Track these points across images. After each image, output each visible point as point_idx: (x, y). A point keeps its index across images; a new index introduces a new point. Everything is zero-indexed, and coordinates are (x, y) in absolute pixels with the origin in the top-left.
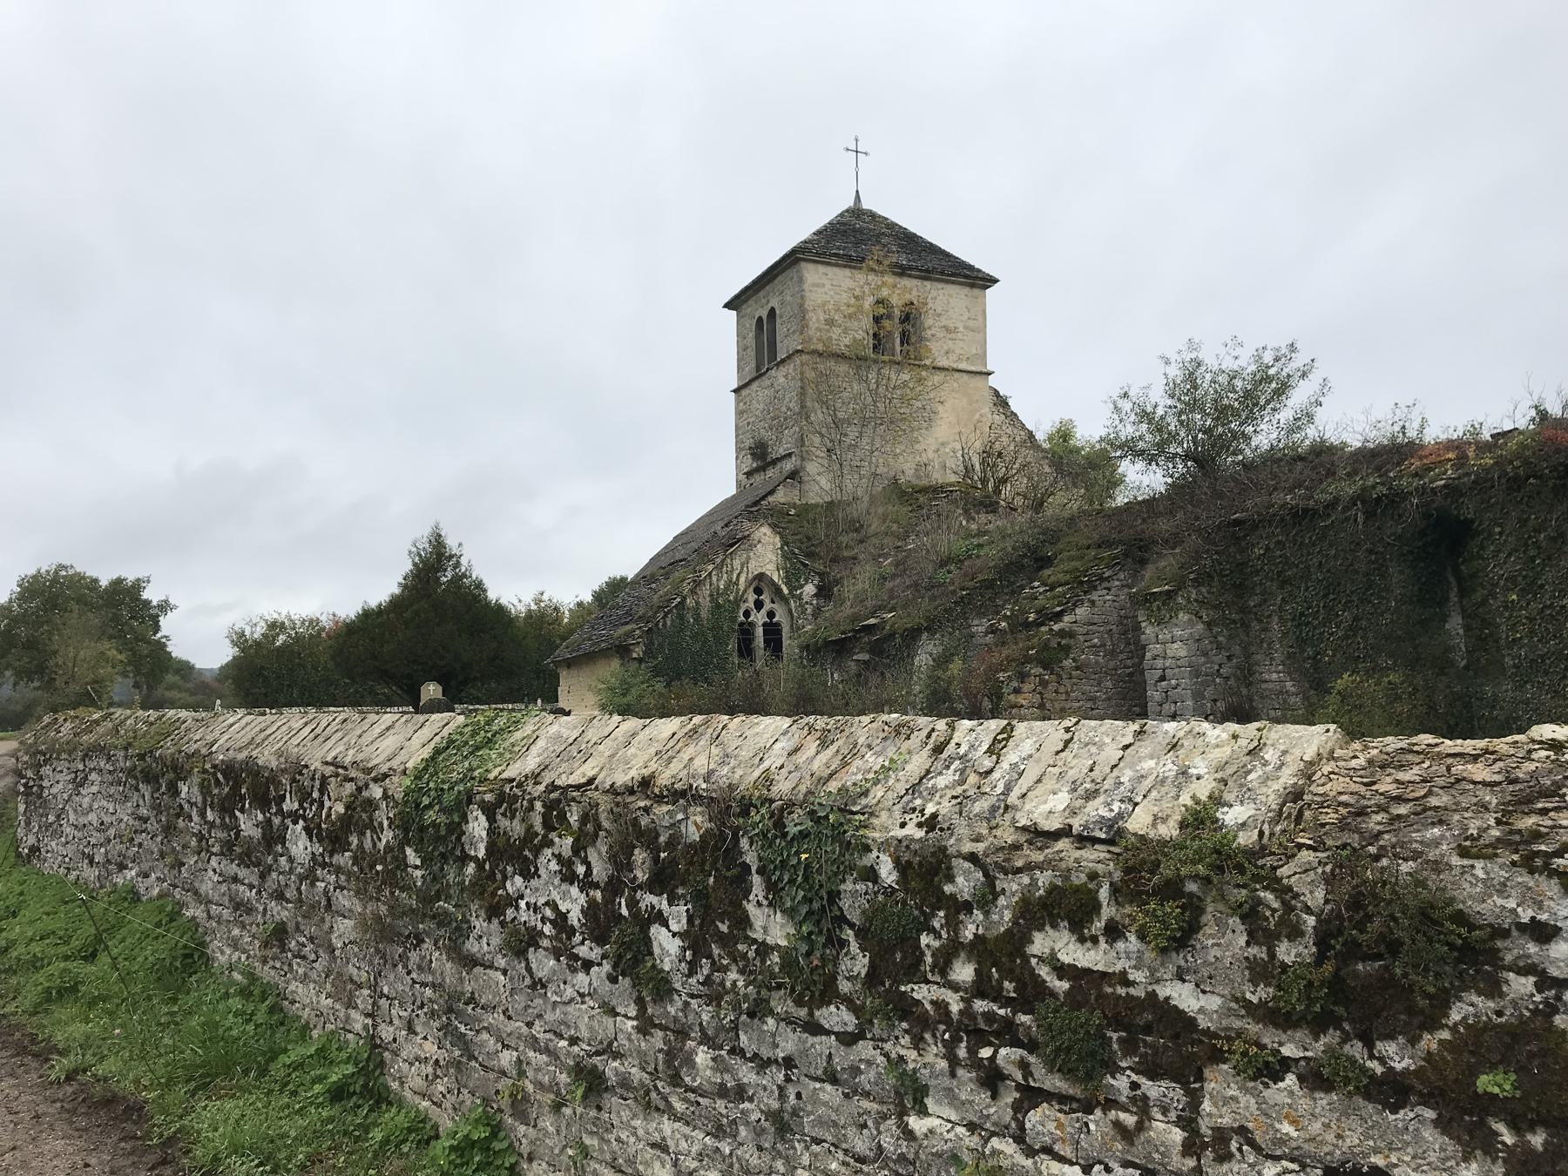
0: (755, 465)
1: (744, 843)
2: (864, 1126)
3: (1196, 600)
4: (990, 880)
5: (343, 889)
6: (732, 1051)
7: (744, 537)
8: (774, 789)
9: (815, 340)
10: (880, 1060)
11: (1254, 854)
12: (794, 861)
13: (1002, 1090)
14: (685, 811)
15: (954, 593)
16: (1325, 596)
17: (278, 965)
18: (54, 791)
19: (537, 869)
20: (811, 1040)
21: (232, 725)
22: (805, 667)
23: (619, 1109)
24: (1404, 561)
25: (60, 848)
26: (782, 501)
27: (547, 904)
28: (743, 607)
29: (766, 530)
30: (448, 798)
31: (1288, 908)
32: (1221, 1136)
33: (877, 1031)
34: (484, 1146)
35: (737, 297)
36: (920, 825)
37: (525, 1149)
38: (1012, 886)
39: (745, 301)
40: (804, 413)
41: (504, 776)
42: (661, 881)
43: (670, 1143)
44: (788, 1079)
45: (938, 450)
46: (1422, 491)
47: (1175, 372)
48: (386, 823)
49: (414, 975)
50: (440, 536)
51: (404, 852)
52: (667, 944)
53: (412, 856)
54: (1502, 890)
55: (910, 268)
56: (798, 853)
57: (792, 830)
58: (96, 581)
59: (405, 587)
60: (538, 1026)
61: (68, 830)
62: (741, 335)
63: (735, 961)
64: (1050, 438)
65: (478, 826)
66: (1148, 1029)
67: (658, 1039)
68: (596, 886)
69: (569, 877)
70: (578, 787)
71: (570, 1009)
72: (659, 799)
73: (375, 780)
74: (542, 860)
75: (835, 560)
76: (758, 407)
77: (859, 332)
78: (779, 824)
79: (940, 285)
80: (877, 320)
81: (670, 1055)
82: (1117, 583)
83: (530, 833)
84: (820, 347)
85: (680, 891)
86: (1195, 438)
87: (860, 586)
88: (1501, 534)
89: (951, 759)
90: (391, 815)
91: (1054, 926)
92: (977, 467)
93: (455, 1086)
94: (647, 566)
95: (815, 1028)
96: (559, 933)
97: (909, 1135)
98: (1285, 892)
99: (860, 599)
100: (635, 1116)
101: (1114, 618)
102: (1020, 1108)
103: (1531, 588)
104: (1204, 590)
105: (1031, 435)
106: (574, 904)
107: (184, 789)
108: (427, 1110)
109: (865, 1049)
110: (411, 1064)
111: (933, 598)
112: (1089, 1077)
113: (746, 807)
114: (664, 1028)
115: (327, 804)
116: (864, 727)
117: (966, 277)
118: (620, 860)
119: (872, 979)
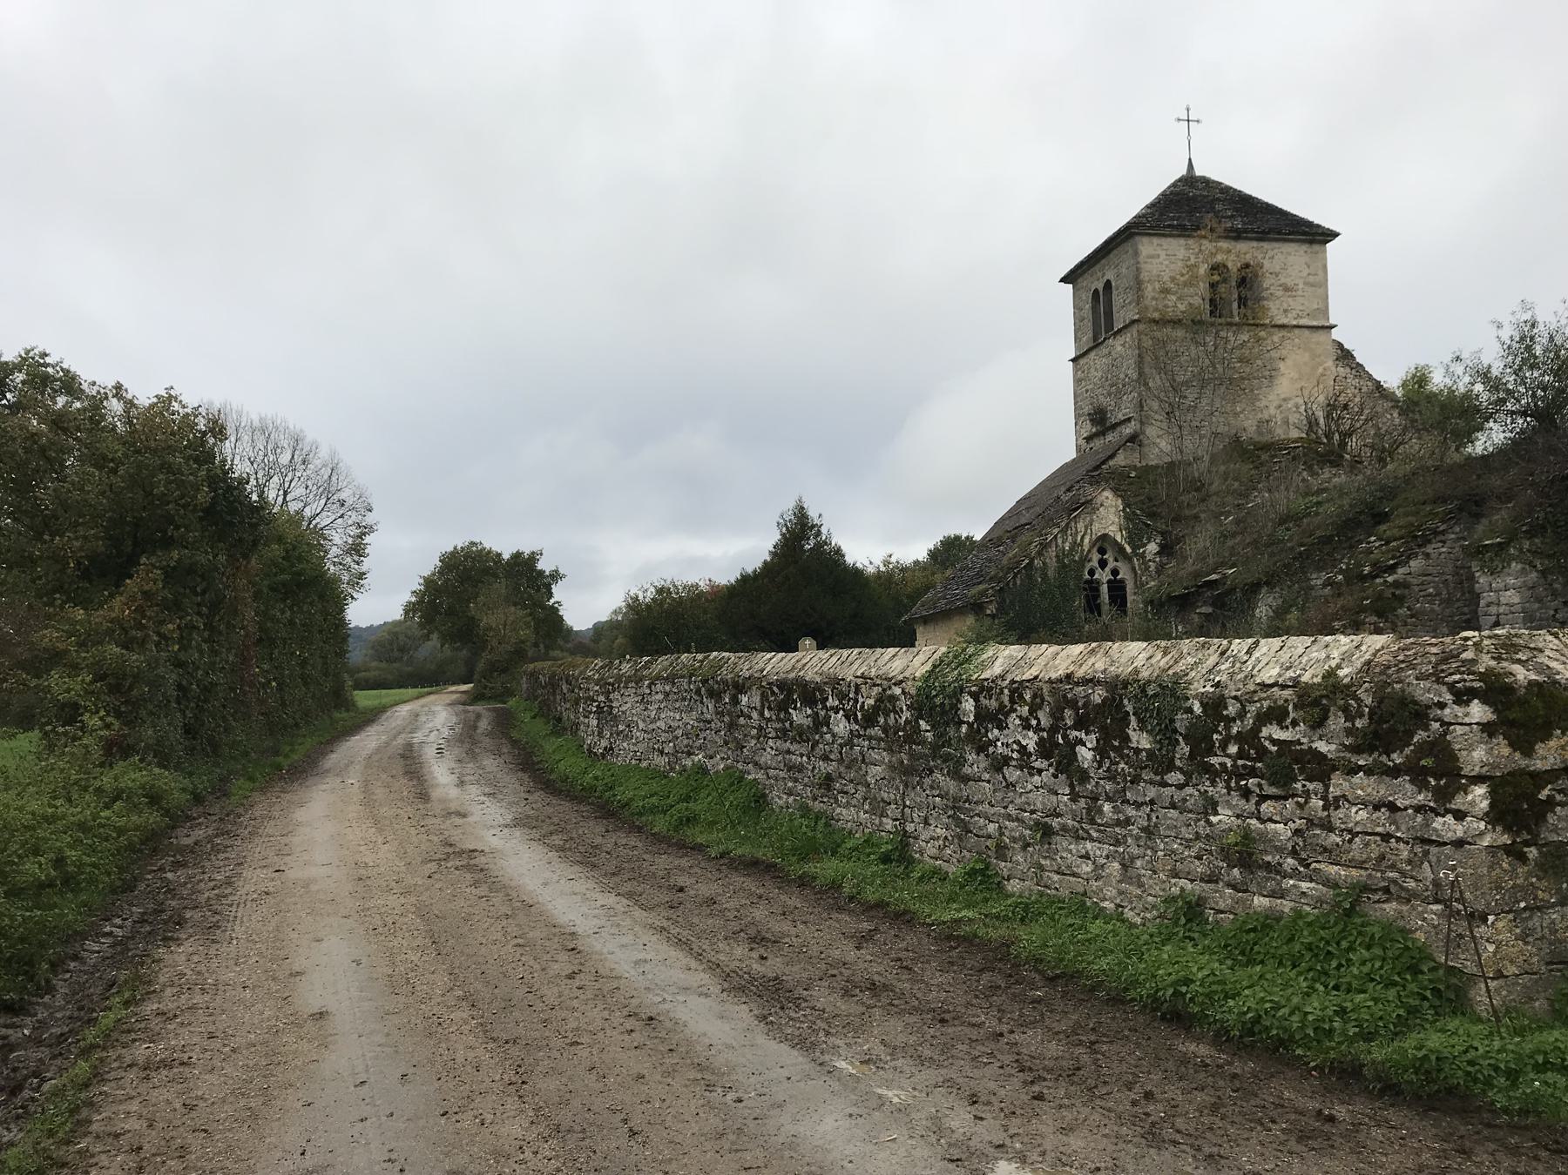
0: (1094, 430)
1: (1126, 702)
2: (1190, 825)
3: (1528, 551)
4: (1243, 707)
6: (1122, 802)
8: (1140, 675)
10: (1196, 793)
11: (1348, 686)
13: (1251, 797)
14: (1093, 689)
15: (1292, 548)
17: (825, 800)
18: (624, 708)
21: (771, 659)
22: (1149, 620)
23: (1061, 842)
25: (631, 747)
26: (1123, 464)
27: (1014, 742)
28: (1088, 566)
29: (1108, 493)
32: (1336, 799)
34: (983, 872)
35: (1072, 272)
36: (1212, 686)
37: (1006, 873)
38: (1252, 708)
42: (1080, 724)
43: (1091, 853)
44: (1152, 810)
45: (1280, 406)
47: (1506, 333)
48: (904, 708)
49: (928, 792)
50: (803, 508)
51: (918, 723)
52: (1085, 755)
53: (923, 724)
54: (1429, 691)
55: (1246, 231)
56: (1153, 704)
58: (499, 555)
59: (774, 554)
60: (1010, 807)
61: (638, 734)
62: (1077, 307)
64: (1404, 385)
65: (968, 705)
66: (1309, 763)
67: (1082, 803)
68: (1044, 730)
69: (1026, 726)
70: (1028, 681)
71: (1030, 795)
72: (1077, 684)
73: (895, 684)
74: (1010, 719)
75: (1177, 519)
77: (1197, 297)
78: (1144, 691)
79: (1276, 245)
80: (1213, 286)
81: (1089, 810)
82: (1453, 536)
84: (1156, 315)
86: (1534, 395)
87: (1200, 545)
91: (1271, 724)
92: (1322, 421)
93: (958, 850)
94: (992, 530)
95: (1165, 784)
98: (1358, 700)
99: (1202, 557)
100: (1070, 844)
101: (1449, 569)
102: (1258, 804)
104: (1537, 540)
105: (1378, 385)
106: (1031, 741)
107: (744, 699)
109: (1189, 790)
110: (927, 842)
111: (1272, 555)
112: (1285, 785)
113: (1126, 684)
114: (1084, 797)
115: (861, 700)
116: (1186, 645)
117: (1305, 233)
118: (1057, 715)
119: (1192, 756)
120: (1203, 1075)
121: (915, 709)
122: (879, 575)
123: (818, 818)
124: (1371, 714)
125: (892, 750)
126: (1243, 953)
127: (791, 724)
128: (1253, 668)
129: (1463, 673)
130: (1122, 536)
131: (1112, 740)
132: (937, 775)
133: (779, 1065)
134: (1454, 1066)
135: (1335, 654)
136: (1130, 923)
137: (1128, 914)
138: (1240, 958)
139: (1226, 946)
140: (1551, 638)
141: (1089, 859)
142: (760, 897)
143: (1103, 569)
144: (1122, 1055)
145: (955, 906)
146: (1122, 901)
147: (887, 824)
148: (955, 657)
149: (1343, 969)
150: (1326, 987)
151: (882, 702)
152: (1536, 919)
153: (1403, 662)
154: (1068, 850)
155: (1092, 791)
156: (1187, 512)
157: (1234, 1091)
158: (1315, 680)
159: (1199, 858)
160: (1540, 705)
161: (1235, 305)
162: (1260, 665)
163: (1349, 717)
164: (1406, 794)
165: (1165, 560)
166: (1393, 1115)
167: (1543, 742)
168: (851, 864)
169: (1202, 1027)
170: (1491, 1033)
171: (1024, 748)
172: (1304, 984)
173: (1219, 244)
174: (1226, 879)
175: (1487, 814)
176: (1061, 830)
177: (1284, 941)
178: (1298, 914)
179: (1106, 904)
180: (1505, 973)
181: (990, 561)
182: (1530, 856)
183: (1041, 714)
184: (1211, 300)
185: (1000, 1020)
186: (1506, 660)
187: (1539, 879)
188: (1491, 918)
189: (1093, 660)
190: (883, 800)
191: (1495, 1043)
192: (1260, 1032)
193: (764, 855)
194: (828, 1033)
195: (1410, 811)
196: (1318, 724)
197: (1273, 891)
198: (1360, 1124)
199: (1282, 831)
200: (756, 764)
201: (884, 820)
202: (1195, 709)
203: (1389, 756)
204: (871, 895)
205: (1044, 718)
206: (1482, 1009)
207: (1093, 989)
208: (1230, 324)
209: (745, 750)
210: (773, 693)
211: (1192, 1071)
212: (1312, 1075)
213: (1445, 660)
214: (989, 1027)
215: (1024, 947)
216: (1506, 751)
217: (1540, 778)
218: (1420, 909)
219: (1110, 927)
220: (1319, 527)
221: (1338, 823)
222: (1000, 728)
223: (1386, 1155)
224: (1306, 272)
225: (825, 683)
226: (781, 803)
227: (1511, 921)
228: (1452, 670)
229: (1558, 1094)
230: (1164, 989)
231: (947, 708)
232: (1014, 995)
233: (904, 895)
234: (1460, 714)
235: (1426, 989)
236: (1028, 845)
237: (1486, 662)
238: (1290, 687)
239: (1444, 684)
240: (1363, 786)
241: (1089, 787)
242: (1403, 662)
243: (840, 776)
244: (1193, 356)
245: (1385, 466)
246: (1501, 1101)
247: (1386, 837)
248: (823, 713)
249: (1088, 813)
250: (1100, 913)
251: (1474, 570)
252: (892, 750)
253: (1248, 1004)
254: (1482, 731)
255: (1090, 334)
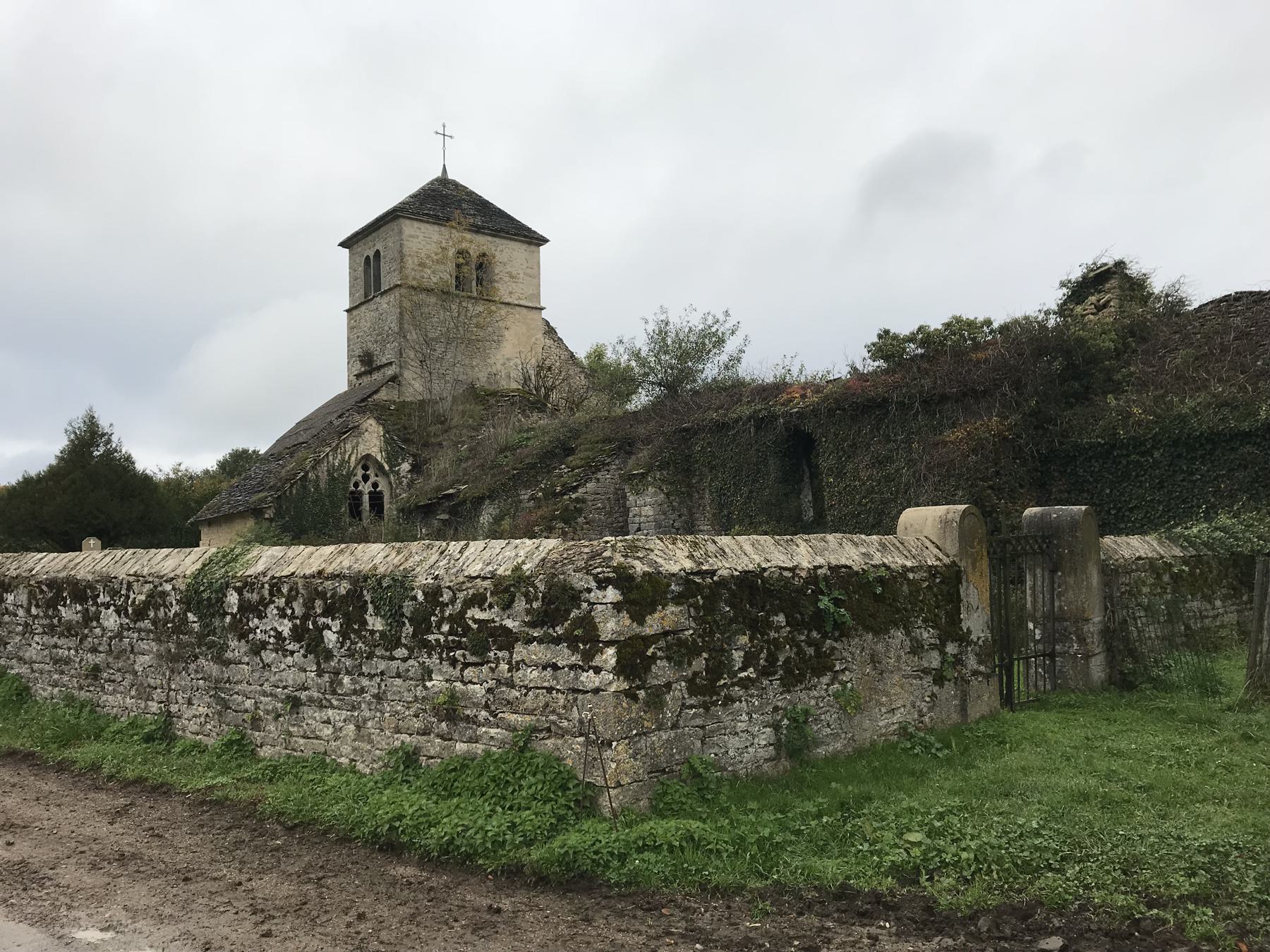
0: (363, 369)
1: (365, 592)
4: (455, 594)
5: (142, 640)
7: (355, 427)
8: (378, 571)
9: (411, 278)
10: (417, 664)
11: (528, 578)
12: (385, 597)
14: (339, 582)
16: (734, 477)
17: (92, 689)
19: (266, 614)
20: (391, 663)
21: (42, 559)
23: (307, 711)
24: (777, 457)
26: (385, 398)
27: (272, 629)
28: (353, 480)
29: (372, 421)
30: (216, 586)
31: (536, 592)
32: (518, 663)
33: (415, 654)
34: (238, 742)
38: (461, 595)
39: (357, 242)
40: (402, 333)
41: (246, 574)
42: (328, 612)
43: (332, 719)
44: (382, 680)
45: (505, 364)
46: (784, 415)
47: (651, 327)
48: (174, 602)
49: (192, 676)
50: (93, 417)
52: (331, 637)
53: (191, 617)
54: (581, 580)
57: (385, 585)
59: (61, 459)
63: (361, 639)
64: (588, 357)
65: (233, 598)
67: (326, 677)
68: (297, 618)
69: (283, 615)
70: (286, 577)
71: (283, 673)
72: (327, 579)
73: (166, 581)
74: (269, 610)
75: (425, 445)
76: (365, 325)
77: (443, 274)
78: (380, 584)
79: (504, 241)
80: (458, 266)
81: (332, 683)
82: (614, 467)
83: (262, 599)
84: (414, 283)
85: (337, 615)
86: (666, 371)
87: (442, 466)
88: (825, 442)
89: (446, 556)
90: (178, 598)
91: (474, 607)
92: (533, 378)
94: (274, 446)
95: (393, 658)
96: (278, 641)
97: (426, 688)
98: (535, 588)
99: (443, 475)
100: (315, 712)
102: (462, 670)
103: (840, 475)
104: (665, 473)
105: (572, 355)
106: (285, 627)
108: (200, 739)
109: (411, 662)
110: (189, 720)
111: (494, 476)
113: (366, 578)
115: (132, 596)
116: (414, 546)
117: (525, 236)
118: (309, 605)
119: (414, 635)
120: (406, 892)
121: (184, 603)
122: (168, 481)
123: (83, 706)
124: (543, 598)
125: (161, 641)
126: (445, 789)
127: (60, 620)
128: (464, 564)
129: (603, 567)
130: (382, 456)
131: (353, 624)
132: (202, 661)
133: (16, 944)
134: (585, 857)
135: (522, 553)
136: (361, 774)
137: (360, 766)
138: (443, 793)
139: (433, 785)
140: (658, 541)
141: (330, 723)
142: (14, 786)
143: (365, 483)
144: (343, 885)
145: (210, 774)
146: (355, 756)
147: (153, 707)
148: (224, 556)
149: (516, 794)
150: (503, 808)
151: (153, 597)
152: (642, 741)
153: (566, 559)
154: (312, 716)
155: (334, 667)
156: (433, 440)
157: (429, 901)
158: (507, 573)
159: (416, 716)
160: (650, 589)
161: (474, 283)
162: (469, 562)
163: (529, 601)
164: (565, 656)
165: (415, 476)
166: (542, 901)
167: (650, 615)
168: (113, 746)
169: (410, 853)
170: (611, 829)
171: (280, 633)
172: (488, 809)
173: (465, 235)
174: (436, 731)
175: (614, 668)
176: (309, 701)
177: (476, 776)
178: (488, 754)
179: (343, 760)
180: (622, 783)
181: (270, 472)
182: (640, 696)
183: (295, 605)
184: (457, 277)
185: (240, 871)
186: (630, 557)
187: (645, 712)
188: (614, 744)
189: (341, 558)
190: (149, 686)
191: (612, 836)
192: (453, 851)
193: (23, 745)
194: (69, 907)
195: (566, 669)
196: (507, 606)
197: (471, 738)
198: (519, 911)
199: (478, 690)
200: (20, 659)
201: (150, 703)
202: (419, 597)
203: (554, 629)
204: (129, 773)
205: (298, 608)
206: (606, 812)
207: (325, 833)
208: (469, 297)
209: (8, 646)
210: (42, 591)
211: (398, 890)
212: (488, 879)
213: (592, 558)
214: (230, 879)
215: (269, 804)
216: (628, 622)
217: (647, 640)
218: (570, 741)
219: (344, 779)
220: (527, 456)
221: (517, 681)
222: (260, 618)
223: (534, 932)
224: (525, 265)
225: (97, 581)
226: (45, 694)
227: (626, 745)
228: (596, 565)
229: (650, 867)
230: (382, 825)
231: (214, 601)
232: (256, 847)
233: (161, 770)
234: (600, 597)
235: (571, 801)
236: (280, 716)
237: (618, 559)
238: (489, 578)
239: (592, 574)
240: (537, 652)
241: (333, 664)
242: (566, 559)
243: (108, 666)
244: (441, 318)
245: (574, 414)
246: (613, 876)
247: (550, 690)
248: (93, 609)
249: (331, 686)
250: (337, 768)
251: (626, 491)
252: (161, 641)
253: (445, 830)
254: (614, 608)
255: (362, 292)
